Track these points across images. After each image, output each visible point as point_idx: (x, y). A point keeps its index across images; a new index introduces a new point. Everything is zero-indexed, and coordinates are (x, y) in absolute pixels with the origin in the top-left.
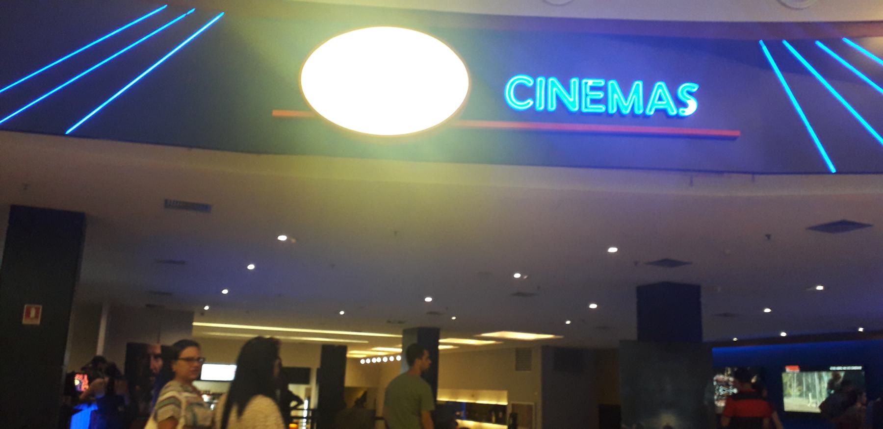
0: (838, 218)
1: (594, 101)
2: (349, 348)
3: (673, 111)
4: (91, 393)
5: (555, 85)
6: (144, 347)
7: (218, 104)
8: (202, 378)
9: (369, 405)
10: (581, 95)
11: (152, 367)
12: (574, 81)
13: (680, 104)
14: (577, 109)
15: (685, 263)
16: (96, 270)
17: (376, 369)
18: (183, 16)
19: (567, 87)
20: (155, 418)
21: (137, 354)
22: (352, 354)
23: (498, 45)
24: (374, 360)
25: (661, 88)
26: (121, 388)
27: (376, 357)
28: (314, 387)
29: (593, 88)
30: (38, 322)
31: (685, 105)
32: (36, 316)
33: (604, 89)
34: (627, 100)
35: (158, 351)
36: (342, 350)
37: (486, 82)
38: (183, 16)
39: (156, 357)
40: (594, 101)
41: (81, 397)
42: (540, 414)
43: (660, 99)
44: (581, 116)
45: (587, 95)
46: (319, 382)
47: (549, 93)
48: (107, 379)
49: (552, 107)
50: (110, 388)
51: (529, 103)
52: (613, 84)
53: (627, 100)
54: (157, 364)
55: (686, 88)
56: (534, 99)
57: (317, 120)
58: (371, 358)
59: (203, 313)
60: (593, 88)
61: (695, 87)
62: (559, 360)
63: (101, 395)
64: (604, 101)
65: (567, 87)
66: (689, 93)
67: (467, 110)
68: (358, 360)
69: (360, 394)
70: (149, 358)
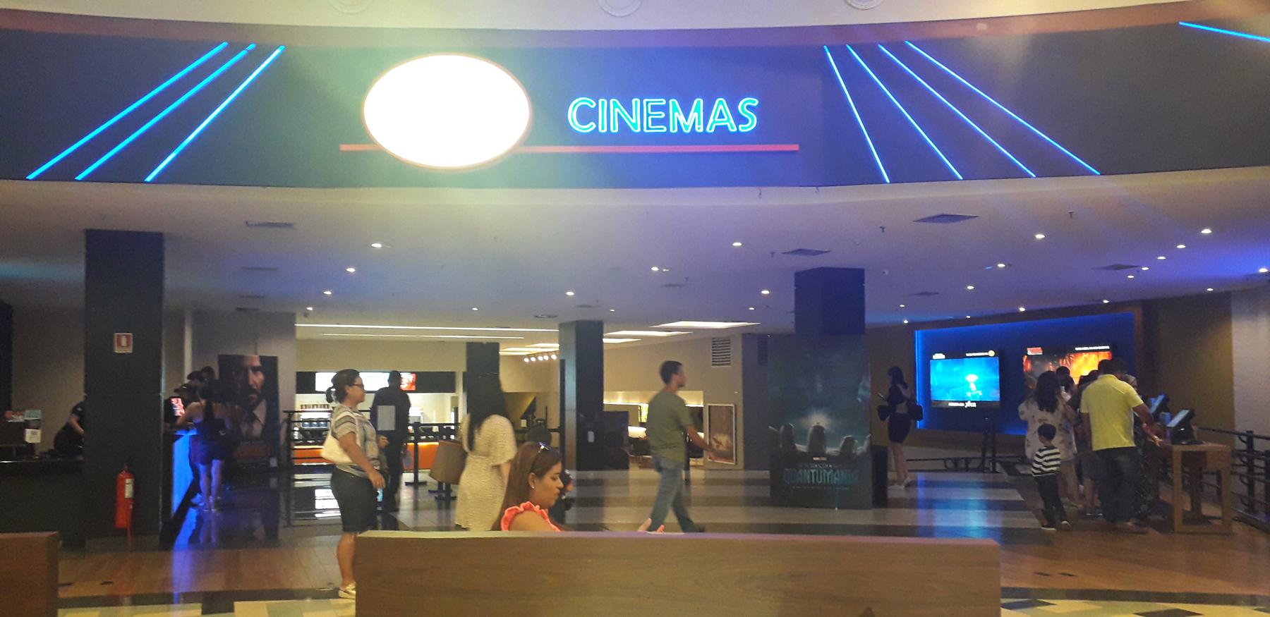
0: (939, 213)
1: (655, 122)
2: (501, 346)
3: (733, 128)
4: (189, 418)
5: (616, 107)
6: (241, 358)
7: (286, 121)
8: (317, 389)
9: (540, 414)
10: (640, 116)
11: (251, 383)
12: (636, 102)
13: (740, 119)
14: (639, 130)
15: (822, 252)
16: (177, 280)
17: (538, 370)
18: (243, 53)
19: (629, 108)
20: (334, 435)
21: (233, 366)
22: (504, 351)
23: (557, 66)
24: (540, 358)
25: (721, 105)
26: (219, 411)
27: (542, 354)
28: (461, 394)
29: (655, 108)
30: (130, 350)
31: (745, 121)
32: (128, 345)
33: (665, 109)
34: (689, 119)
35: (257, 363)
36: (494, 347)
37: (547, 112)
38: (243, 53)
39: (255, 370)
40: (655, 122)
41: (179, 421)
42: (740, 415)
43: (721, 116)
44: (643, 138)
45: (648, 115)
46: (466, 388)
47: (610, 114)
48: (203, 402)
49: (615, 129)
50: (208, 411)
51: (592, 126)
52: (674, 103)
53: (689, 119)
54: (257, 379)
55: (746, 104)
56: (597, 123)
57: (382, 153)
58: (535, 355)
59: (306, 314)
60: (655, 108)
61: (755, 102)
62: (759, 347)
63: (199, 420)
64: (665, 121)
65: (629, 108)
66: (749, 108)
67: (531, 137)
68: (519, 359)
69: (530, 401)
70: (246, 370)
